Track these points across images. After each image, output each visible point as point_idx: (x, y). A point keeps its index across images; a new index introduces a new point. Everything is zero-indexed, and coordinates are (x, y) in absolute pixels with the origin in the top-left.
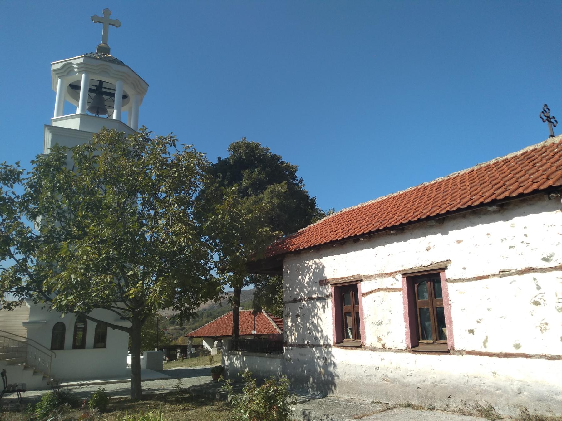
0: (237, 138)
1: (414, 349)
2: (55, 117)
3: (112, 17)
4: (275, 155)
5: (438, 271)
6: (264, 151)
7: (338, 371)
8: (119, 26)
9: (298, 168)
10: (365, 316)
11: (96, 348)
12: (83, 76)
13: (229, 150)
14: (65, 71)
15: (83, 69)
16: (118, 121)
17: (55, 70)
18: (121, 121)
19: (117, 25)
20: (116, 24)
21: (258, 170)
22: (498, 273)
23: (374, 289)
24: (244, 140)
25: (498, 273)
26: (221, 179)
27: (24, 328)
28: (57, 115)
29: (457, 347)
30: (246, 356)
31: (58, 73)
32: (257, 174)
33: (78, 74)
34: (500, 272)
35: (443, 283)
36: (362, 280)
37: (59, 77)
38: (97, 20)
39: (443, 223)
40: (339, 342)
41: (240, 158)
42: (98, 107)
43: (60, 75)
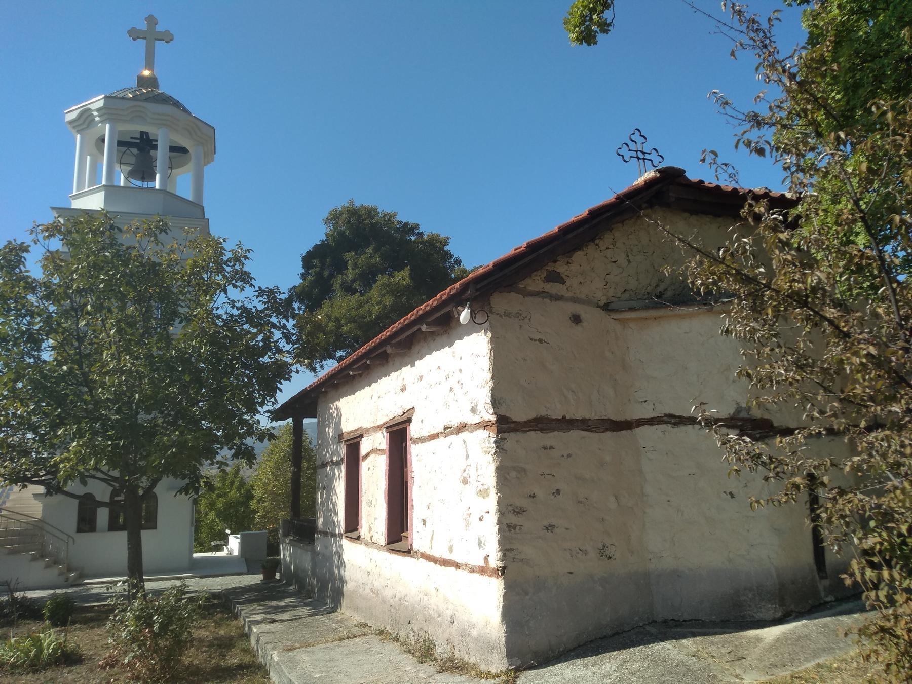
0: (340, 202)
1: (393, 546)
2: (74, 193)
3: (159, 28)
4: (407, 224)
5: (402, 426)
6: (389, 219)
7: (347, 574)
8: (172, 40)
9: (450, 241)
10: (363, 492)
11: (80, 532)
12: (108, 126)
13: (326, 222)
14: (84, 122)
15: (106, 116)
16: (163, 191)
17: (71, 122)
18: (168, 190)
19: (168, 40)
20: (167, 37)
21: (370, 250)
22: (443, 431)
23: (369, 451)
24: (352, 202)
25: (443, 431)
26: (318, 269)
27: (37, 501)
28: (78, 190)
29: (416, 547)
30: (294, 546)
31: (76, 126)
32: (369, 256)
33: (100, 124)
34: (445, 428)
35: (409, 443)
36: (361, 436)
37: (78, 132)
38: (135, 34)
39: (410, 348)
40: (349, 530)
41: (342, 234)
42: (143, 172)
43: (80, 128)
